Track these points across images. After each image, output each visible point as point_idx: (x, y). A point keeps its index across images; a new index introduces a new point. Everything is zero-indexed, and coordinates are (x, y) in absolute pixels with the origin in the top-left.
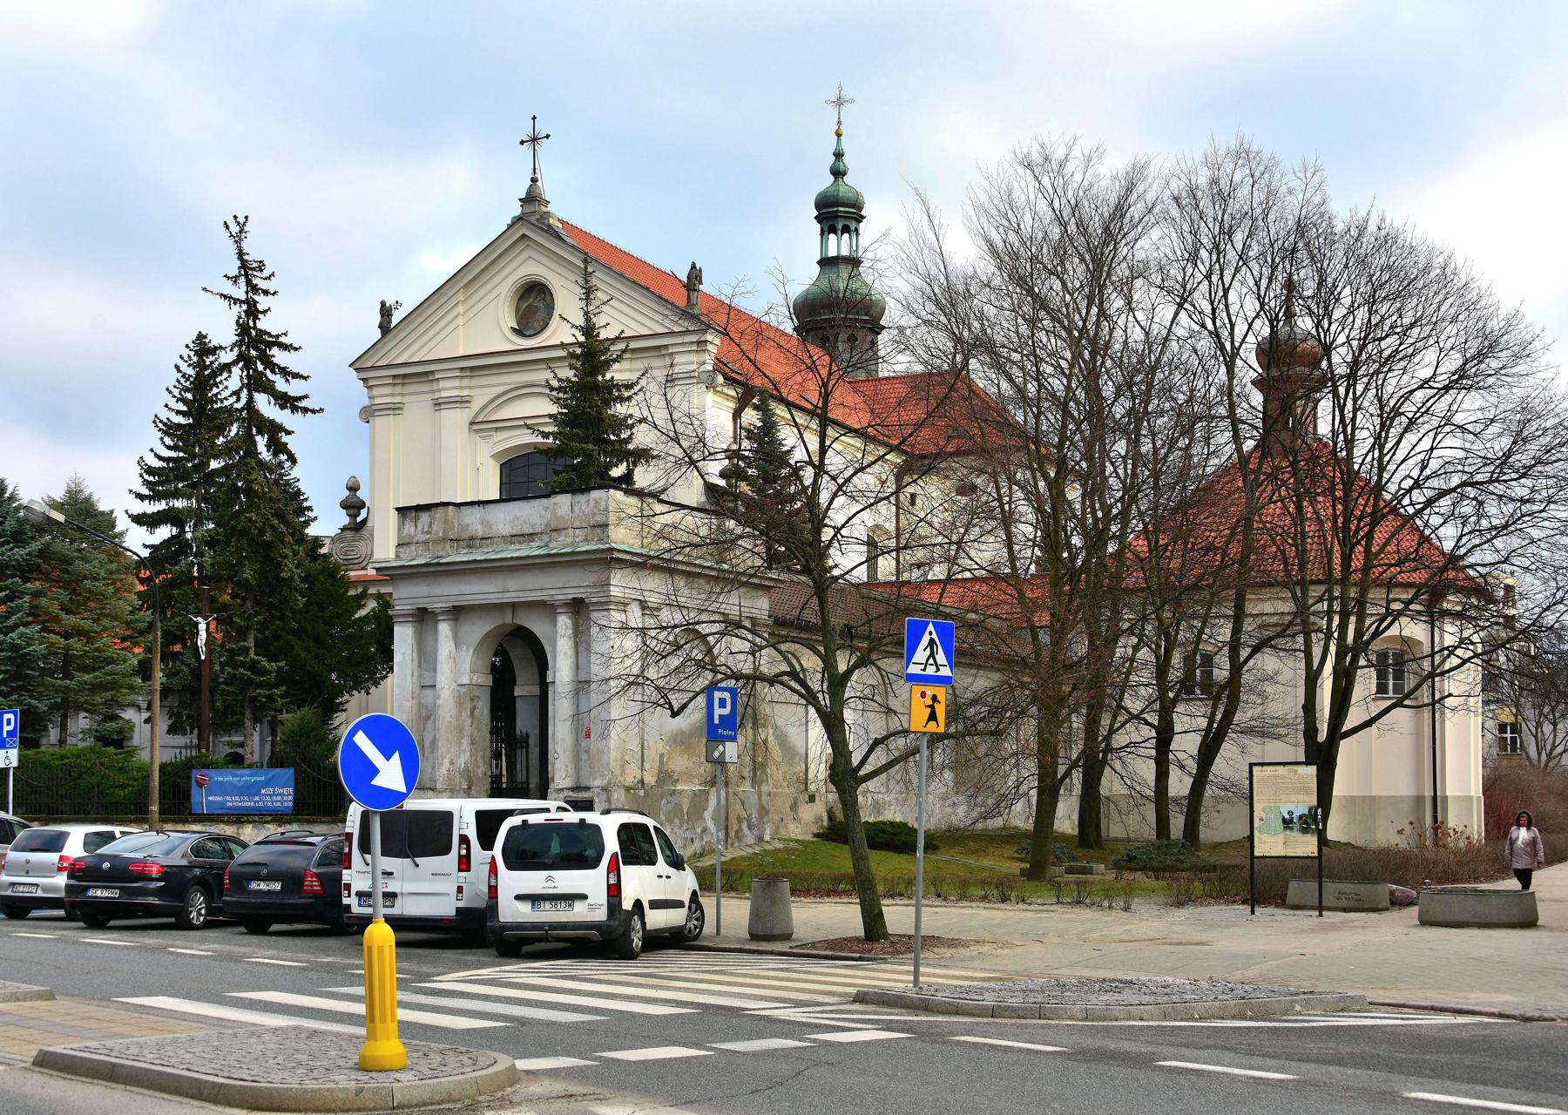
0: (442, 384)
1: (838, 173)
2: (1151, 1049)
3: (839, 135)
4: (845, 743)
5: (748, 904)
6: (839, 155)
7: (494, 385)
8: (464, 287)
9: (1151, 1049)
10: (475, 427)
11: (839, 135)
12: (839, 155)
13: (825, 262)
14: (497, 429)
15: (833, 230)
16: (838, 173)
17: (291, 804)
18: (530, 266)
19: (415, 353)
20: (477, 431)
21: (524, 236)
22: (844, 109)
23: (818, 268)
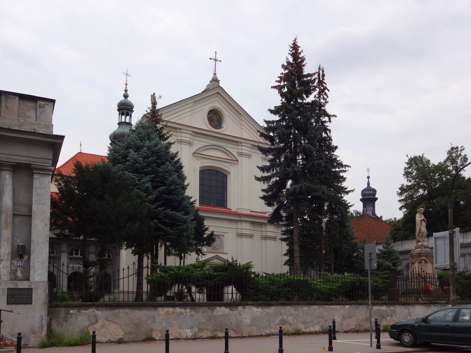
1: (126, 96)
2: (430, 341)
3: (126, 84)
4: (192, 297)
6: (126, 91)
7: (204, 142)
8: (194, 102)
9: (430, 341)
10: (195, 155)
11: (126, 84)
12: (126, 91)
13: (120, 124)
14: (203, 158)
15: (123, 114)
16: (126, 96)
17: (96, 345)
18: (215, 104)
19: (171, 119)
20: (195, 156)
21: (218, 93)
22: (128, 78)
23: (118, 126)
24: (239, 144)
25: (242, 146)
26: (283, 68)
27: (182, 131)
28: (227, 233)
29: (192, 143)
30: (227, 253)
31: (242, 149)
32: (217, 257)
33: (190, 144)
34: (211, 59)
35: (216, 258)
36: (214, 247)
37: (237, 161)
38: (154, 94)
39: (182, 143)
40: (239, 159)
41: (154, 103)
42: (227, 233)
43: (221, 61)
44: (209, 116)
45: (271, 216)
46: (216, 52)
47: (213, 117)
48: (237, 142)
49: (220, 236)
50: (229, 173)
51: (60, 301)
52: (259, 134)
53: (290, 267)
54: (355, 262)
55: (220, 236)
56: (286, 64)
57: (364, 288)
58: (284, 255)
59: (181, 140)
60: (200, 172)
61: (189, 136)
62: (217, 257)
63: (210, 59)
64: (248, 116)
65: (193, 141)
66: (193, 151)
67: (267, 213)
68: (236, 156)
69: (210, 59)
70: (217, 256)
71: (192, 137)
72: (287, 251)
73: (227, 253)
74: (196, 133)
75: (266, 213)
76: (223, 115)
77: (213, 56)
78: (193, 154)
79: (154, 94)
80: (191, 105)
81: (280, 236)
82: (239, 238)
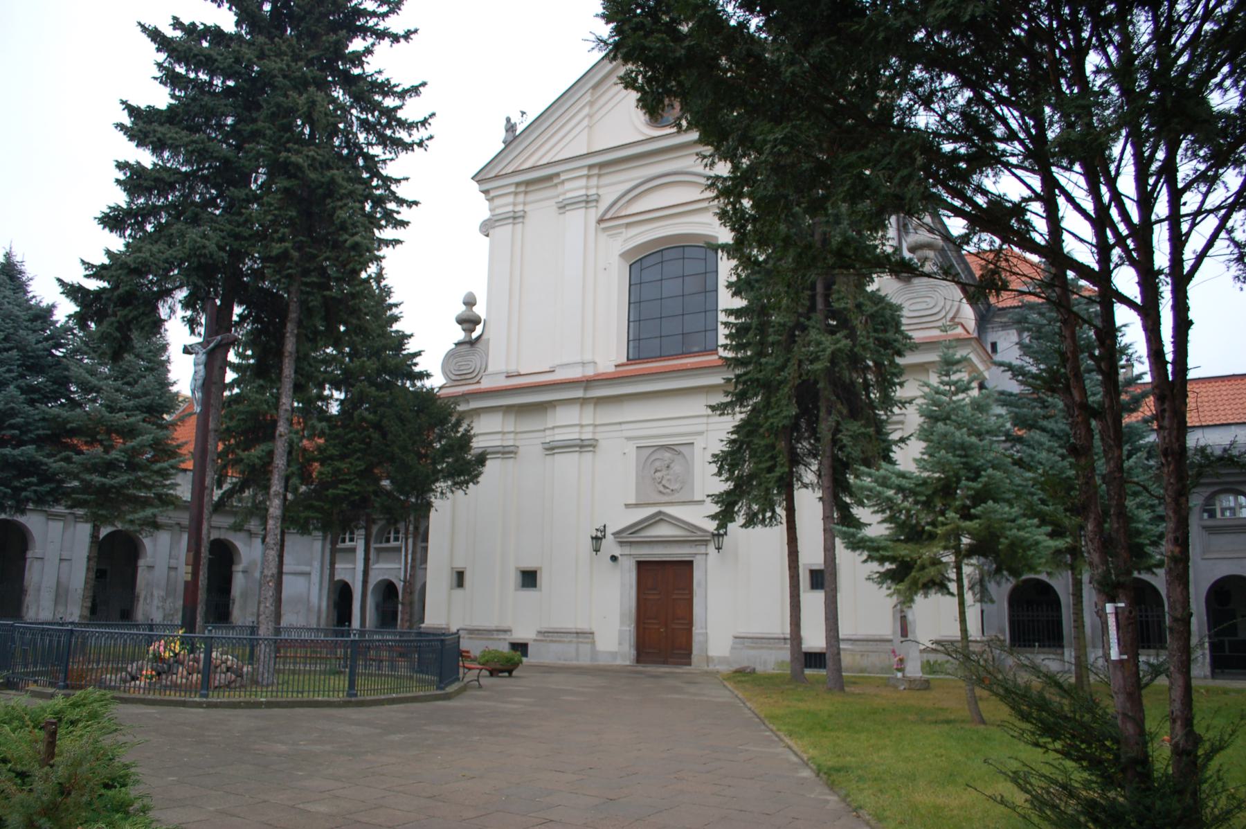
0: (568, 186)
5: (731, 242)
10: (603, 225)
14: (628, 225)
20: (605, 229)
24: (556, 181)
25: (563, 182)
26: (108, 211)
27: (563, 177)
28: (700, 433)
33: (588, 201)
36: (664, 486)
39: (567, 208)
41: (398, 181)
42: (700, 433)
48: (550, 178)
49: (681, 449)
54: (1005, 441)
55: (681, 449)
56: (120, 198)
57: (290, 453)
64: (554, 108)
70: (660, 513)
80: (588, 98)
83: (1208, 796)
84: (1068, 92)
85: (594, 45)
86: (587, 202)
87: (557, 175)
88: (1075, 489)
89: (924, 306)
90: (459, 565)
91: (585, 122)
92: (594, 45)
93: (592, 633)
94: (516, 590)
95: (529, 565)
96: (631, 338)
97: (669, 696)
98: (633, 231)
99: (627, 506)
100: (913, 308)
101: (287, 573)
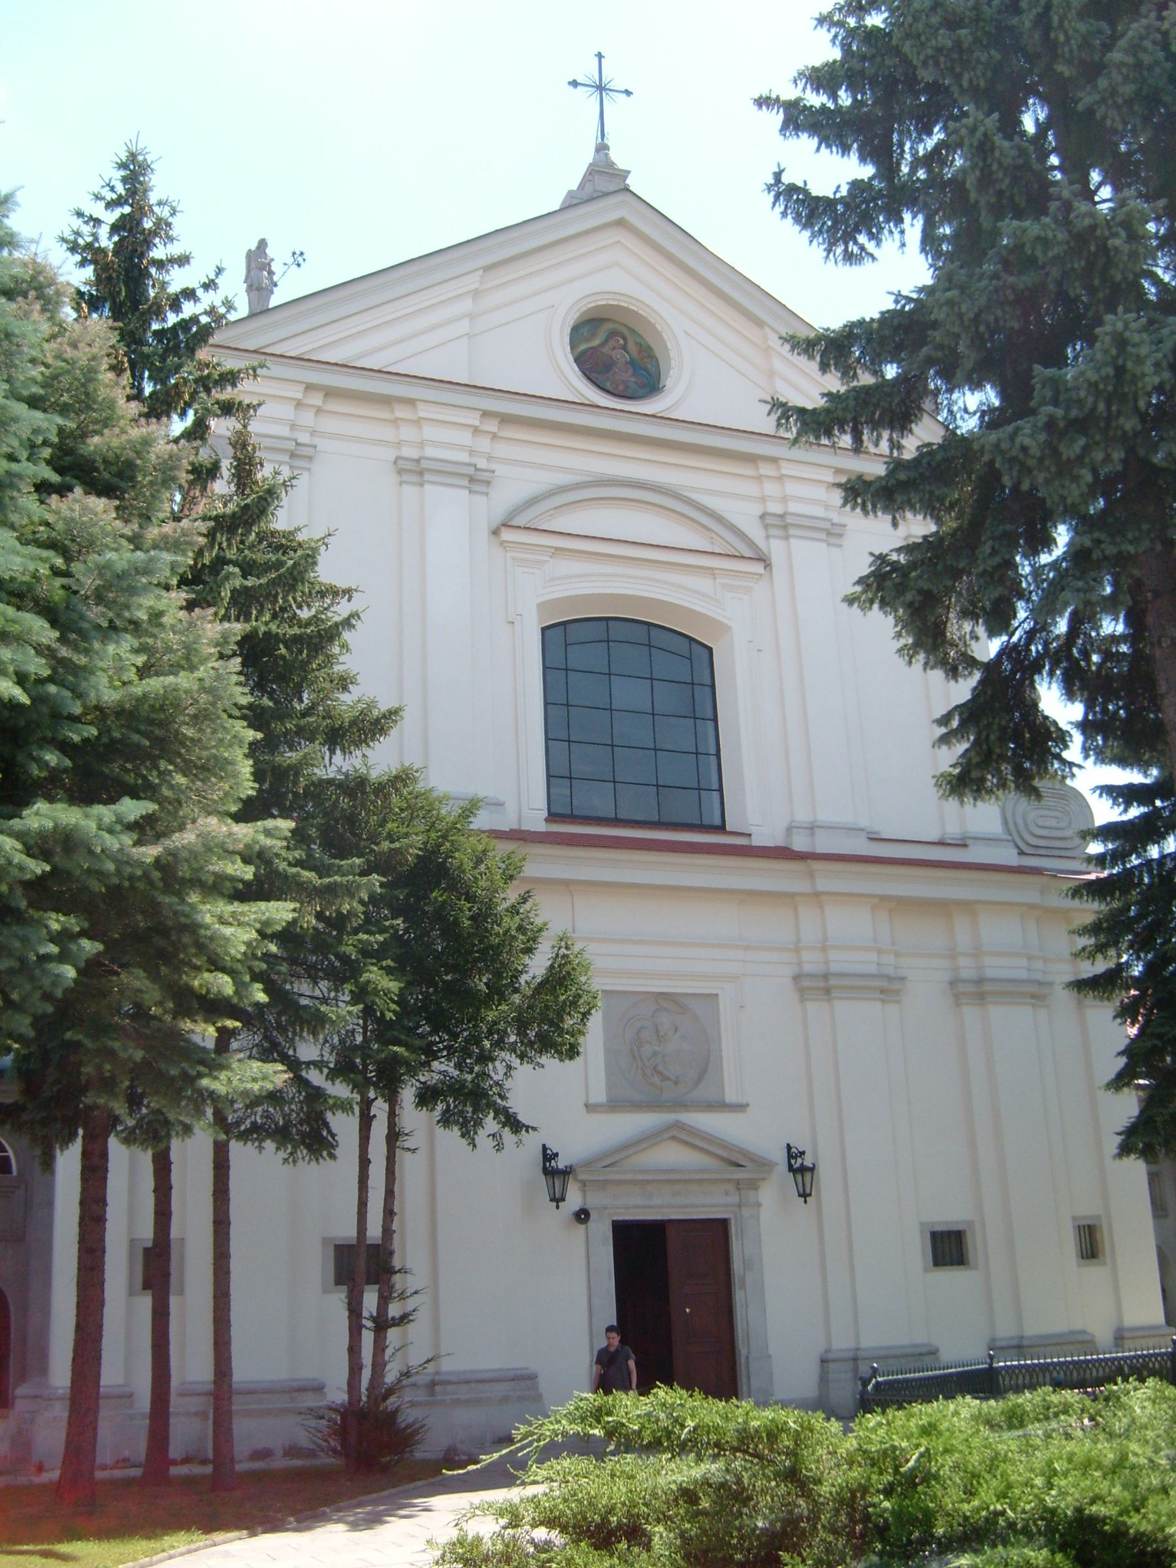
8: (487, 269)
10: (507, 535)
21: (621, 223)
24: (401, 412)
27: (424, 411)
29: (485, 476)
30: (741, 1107)
31: (781, 478)
32: (674, 1133)
34: (574, 84)
35: (674, 1138)
37: (763, 559)
38: (262, 244)
40: (776, 549)
43: (628, 93)
44: (583, 347)
45: (955, 723)
46: (600, 56)
47: (605, 350)
48: (386, 401)
50: (722, 628)
51: (136, 395)
52: (776, 118)
53: (1155, 1168)
58: (1109, 1086)
59: (418, 461)
60: (547, 632)
61: (465, 438)
62: (674, 1133)
63: (570, 83)
65: (493, 466)
66: (498, 516)
67: (969, 842)
68: (756, 533)
69: (570, 83)
70: (678, 1125)
71: (484, 444)
72: (1122, 1061)
73: (741, 1107)
74: (506, 419)
75: (965, 846)
76: (658, 334)
77: (587, 71)
78: (495, 532)
79: (262, 244)
81: (1066, 971)
82: (811, 1006)
83: (833, 1485)
84: (314, 666)
85: (60, 271)
86: (472, 480)
87: (411, 402)
88: (474, 1112)
89: (1053, 823)
90: (1094, 1273)
91: (464, 326)
92: (60, 271)
93: (532, 1378)
94: (325, 1291)
95: (918, 1250)
96: (713, 759)
97: (455, 1472)
98: (566, 566)
99: (590, 1108)
100: (1041, 822)
101: (857, 1336)
